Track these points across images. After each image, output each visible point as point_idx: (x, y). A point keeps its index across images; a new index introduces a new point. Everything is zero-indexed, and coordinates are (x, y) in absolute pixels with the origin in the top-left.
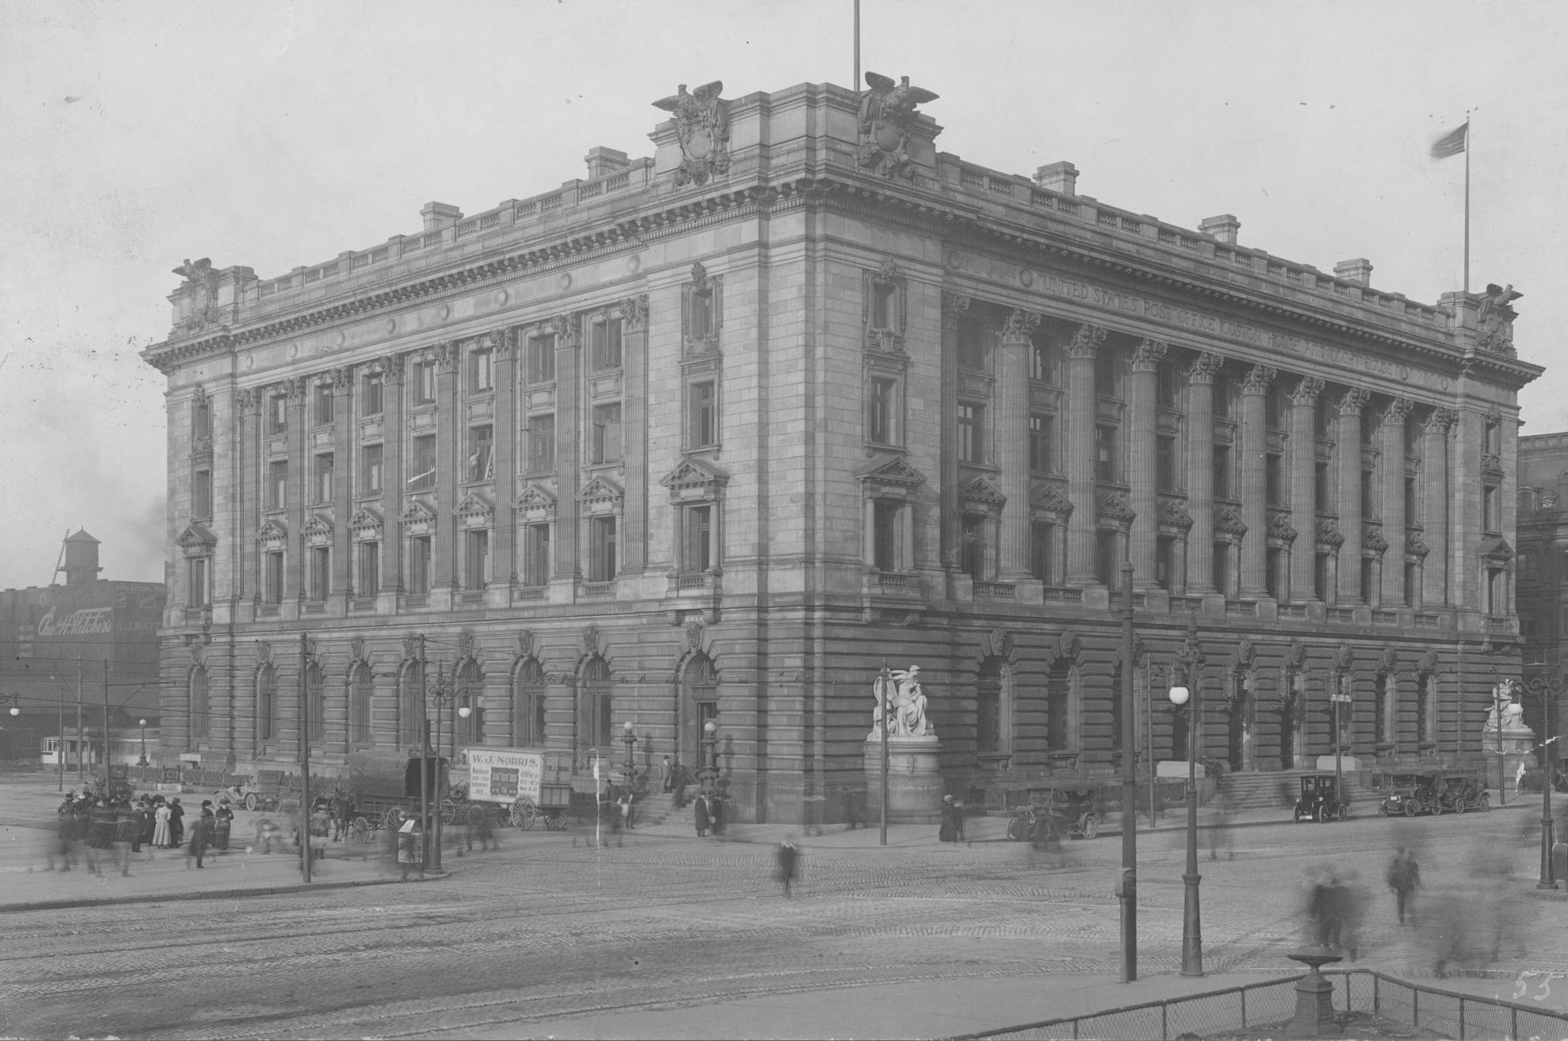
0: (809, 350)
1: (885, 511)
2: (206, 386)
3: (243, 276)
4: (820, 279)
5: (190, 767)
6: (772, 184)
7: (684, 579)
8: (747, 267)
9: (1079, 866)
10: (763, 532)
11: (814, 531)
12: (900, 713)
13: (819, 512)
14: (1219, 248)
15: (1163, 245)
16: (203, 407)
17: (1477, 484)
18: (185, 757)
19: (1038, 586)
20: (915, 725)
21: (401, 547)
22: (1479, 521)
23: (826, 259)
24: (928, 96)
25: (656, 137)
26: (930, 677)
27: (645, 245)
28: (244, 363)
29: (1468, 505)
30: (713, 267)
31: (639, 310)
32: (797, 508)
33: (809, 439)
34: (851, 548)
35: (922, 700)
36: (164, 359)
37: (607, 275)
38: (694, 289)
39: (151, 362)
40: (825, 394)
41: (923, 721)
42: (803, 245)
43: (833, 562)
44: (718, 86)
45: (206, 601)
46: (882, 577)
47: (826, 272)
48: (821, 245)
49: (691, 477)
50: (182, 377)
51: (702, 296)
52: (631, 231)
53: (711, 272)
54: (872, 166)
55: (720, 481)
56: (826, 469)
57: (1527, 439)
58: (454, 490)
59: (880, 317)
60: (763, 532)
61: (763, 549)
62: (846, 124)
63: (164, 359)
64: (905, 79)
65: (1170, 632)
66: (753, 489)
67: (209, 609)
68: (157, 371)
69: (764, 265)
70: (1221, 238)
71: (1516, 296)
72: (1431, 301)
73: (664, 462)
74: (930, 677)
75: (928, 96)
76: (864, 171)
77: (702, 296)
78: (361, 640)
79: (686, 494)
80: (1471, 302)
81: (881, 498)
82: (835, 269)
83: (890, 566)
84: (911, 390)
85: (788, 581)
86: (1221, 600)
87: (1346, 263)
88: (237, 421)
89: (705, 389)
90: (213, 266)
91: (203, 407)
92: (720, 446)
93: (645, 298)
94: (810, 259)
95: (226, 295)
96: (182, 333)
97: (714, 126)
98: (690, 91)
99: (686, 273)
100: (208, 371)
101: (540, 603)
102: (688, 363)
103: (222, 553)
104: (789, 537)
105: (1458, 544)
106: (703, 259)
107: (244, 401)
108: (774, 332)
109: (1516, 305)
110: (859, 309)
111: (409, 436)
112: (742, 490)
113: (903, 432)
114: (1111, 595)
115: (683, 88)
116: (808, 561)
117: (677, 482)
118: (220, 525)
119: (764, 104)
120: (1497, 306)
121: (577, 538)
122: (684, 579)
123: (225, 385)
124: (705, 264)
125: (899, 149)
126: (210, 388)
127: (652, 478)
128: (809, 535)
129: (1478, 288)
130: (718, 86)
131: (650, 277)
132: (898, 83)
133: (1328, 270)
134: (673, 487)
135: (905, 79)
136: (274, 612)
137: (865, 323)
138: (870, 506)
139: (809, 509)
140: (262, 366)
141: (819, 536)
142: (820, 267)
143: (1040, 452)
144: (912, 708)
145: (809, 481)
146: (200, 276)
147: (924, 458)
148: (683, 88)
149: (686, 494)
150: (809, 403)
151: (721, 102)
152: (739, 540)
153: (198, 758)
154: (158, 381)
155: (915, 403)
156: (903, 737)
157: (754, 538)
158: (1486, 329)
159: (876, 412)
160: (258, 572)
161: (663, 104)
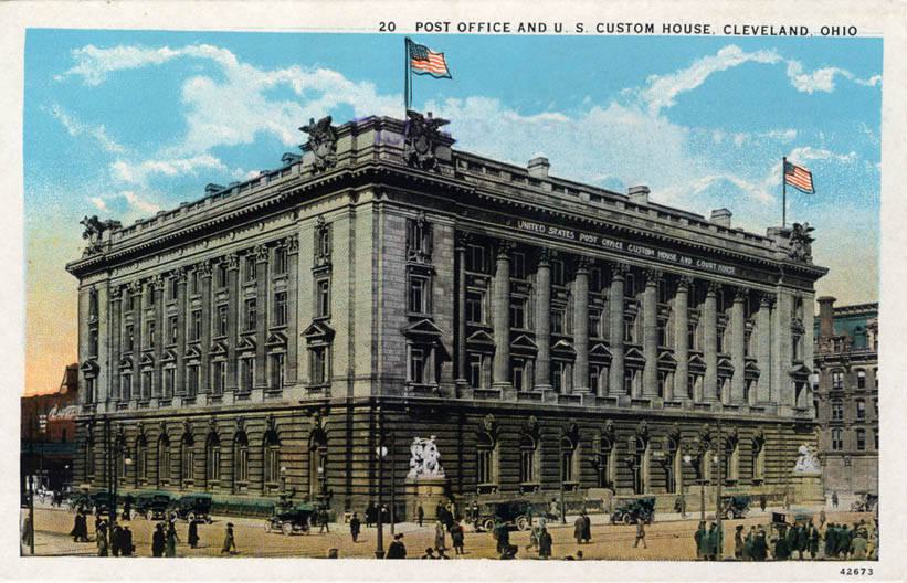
0: (375, 263)
4: (381, 222)
5: (83, 492)
7: (313, 389)
8: (343, 217)
10: (351, 362)
11: (377, 361)
12: (425, 463)
13: (380, 351)
15: (593, 203)
16: (94, 296)
17: (789, 333)
18: (83, 486)
20: (433, 468)
21: (185, 371)
22: (790, 355)
23: (384, 212)
25: (307, 148)
29: (784, 346)
31: (295, 243)
32: (368, 350)
33: (375, 311)
34: (399, 371)
35: (437, 454)
36: (80, 272)
37: (278, 226)
40: (383, 286)
41: (437, 467)
42: (371, 205)
43: (388, 379)
45: (94, 401)
47: (384, 220)
50: (85, 282)
51: (324, 231)
52: (291, 202)
54: (415, 172)
56: (383, 327)
57: (837, 310)
58: (209, 340)
59: (321, 246)
60: (351, 362)
61: (351, 373)
62: (397, 139)
63: (80, 272)
66: (346, 339)
69: (353, 216)
70: (721, 222)
71: (811, 229)
72: (762, 232)
73: (305, 323)
77: (324, 231)
78: (272, 417)
80: (785, 234)
82: (390, 217)
84: (435, 284)
85: (362, 391)
86: (628, 399)
88: (110, 304)
91: (94, 296)
94: (375, 212)
96: (86, 256)
98: (316, 122)
101: (248, 401)
102: (318, 271)
103: (103, 372)
104: (364, 368)
105: (778, 367)
108: (358, 253)
109: (812, 235)
110: (404, 239)
111: (189, 311)
112: (341, 339)
113: (430, 308)
114: (560, 397)
115: (312, 121)
116: (373, 378)
118: (101, 362)
119: (354, 129)
120: (801, 236)
121: (265, 366)
122: (313, 389)
123: (104, 284)
126: (98, 286)
127: (300, 332)
128: (374, 365)
129: (789, 227)
132: (426, 116)
133: (708, 218)
135: (430, 114)
136: (125, 407)
137: (407, 248)
139: (374, 349)
140: (127, 275)
142: (381, 217)
143: (515, 318)
145: (374, 335)
146: (94, 226)
147: (443, 325)
148: (312, 121)
150: (374, 290)
152: (340, 369)
153: (88, 486)
154: (74, 281)
155: (438, 291)
156: (429, 475)
157: (346, 366)
158: (794, 248)
159: (414, 298)
160: (119, 386)
161: (304, 129)
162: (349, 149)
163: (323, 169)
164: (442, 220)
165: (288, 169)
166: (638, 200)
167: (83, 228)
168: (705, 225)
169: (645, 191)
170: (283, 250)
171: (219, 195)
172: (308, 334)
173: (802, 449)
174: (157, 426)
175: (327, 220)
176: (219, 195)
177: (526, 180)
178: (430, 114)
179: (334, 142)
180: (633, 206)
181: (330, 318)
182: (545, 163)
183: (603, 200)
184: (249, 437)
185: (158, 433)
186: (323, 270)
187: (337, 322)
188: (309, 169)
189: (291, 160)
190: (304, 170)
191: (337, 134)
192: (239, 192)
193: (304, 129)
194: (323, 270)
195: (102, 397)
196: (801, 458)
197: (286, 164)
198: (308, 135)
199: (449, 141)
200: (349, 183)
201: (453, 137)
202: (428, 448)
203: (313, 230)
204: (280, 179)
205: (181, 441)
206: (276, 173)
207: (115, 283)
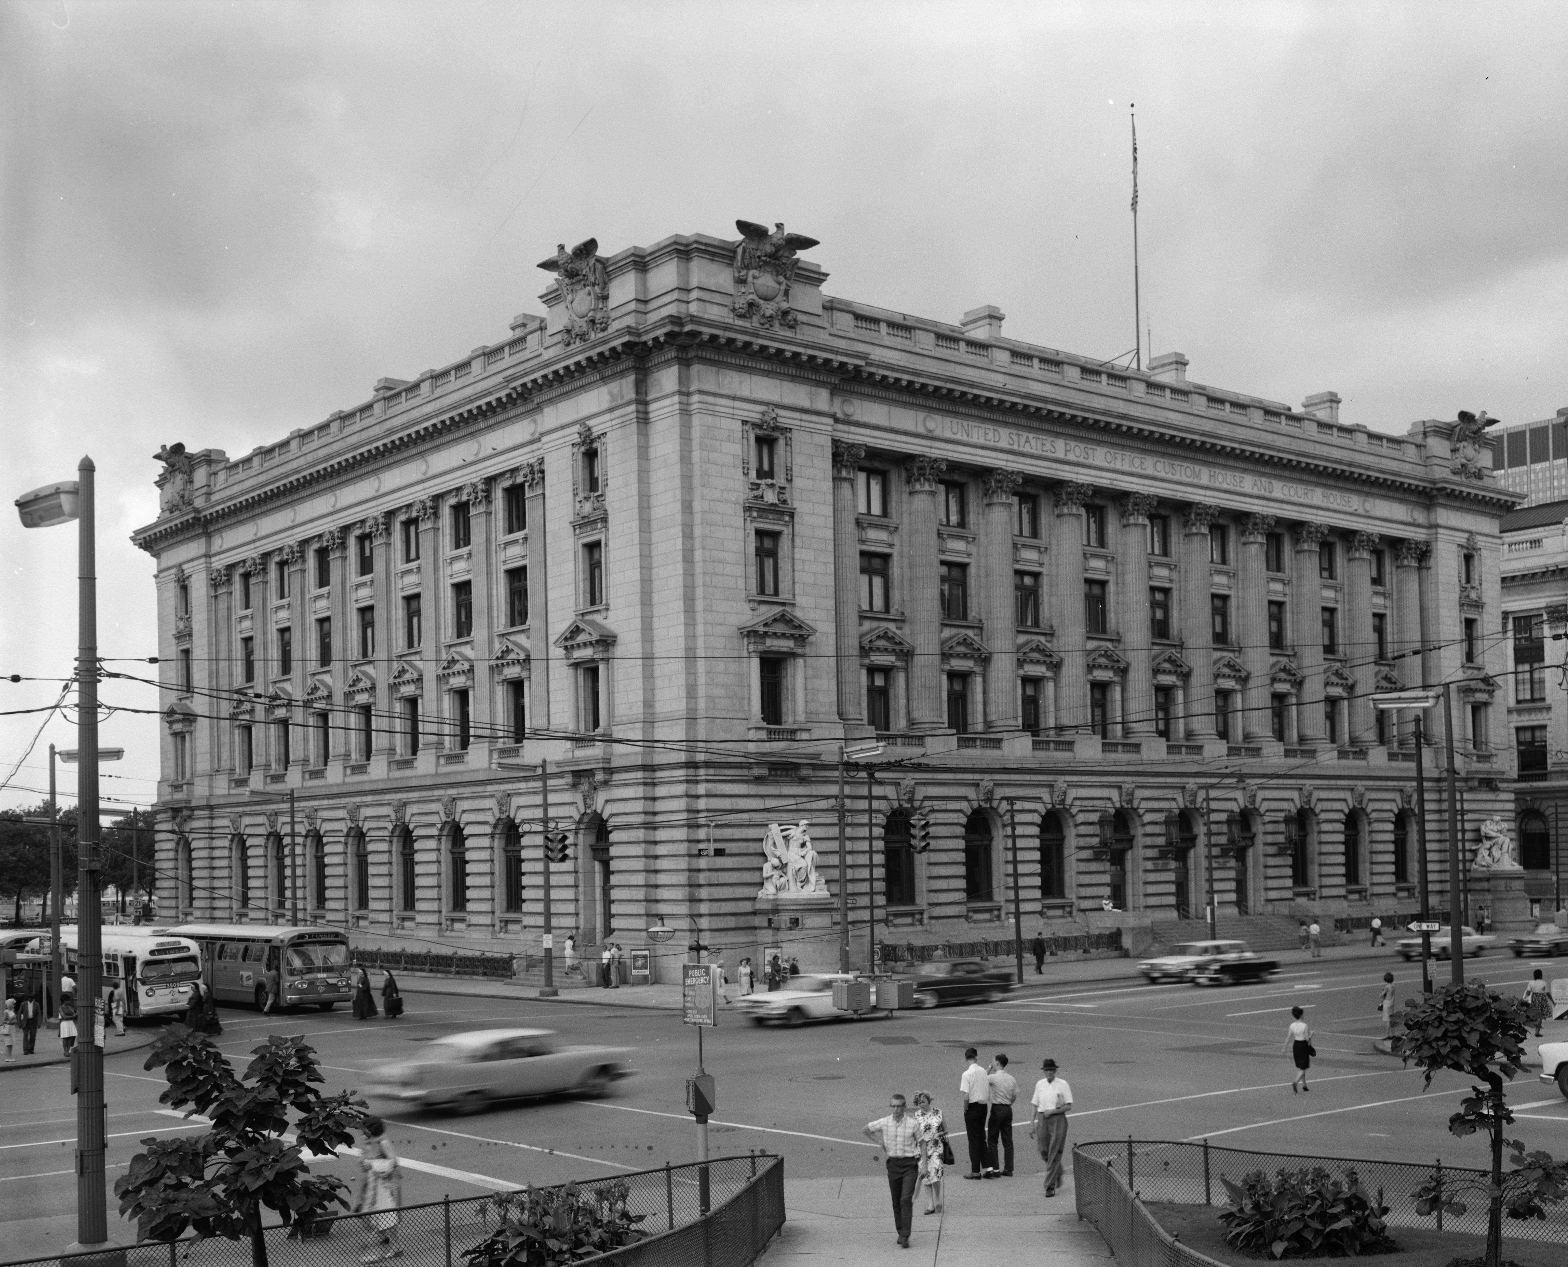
1: (773, 668)
2: (185, 567)
3: (209, 458)
6: (644, 338)
9: (1264, 982)
12: (790, 870)
14: (1323, 426)
19: (1279, 748)
20: (806, 881)
24: (808, 243)
25: (551, 298)
26: (819, 832)
27: (539, 408)
28: (218, 543)
30: (597, 426)
31: (537, 473)
35: (810, 852)
37: (502, 446)
38: (583, 449)
39: (141, 546)
44: (590, 246)
46: (770, 732)
48: (695, 398)
49: (582, 638)
52: (523, 398)
53: (596, 431)
54: (737, 318)
55: (607, 642)
62: (721, 277)
64: (1484, 413)
65: (1390, 783)
67: (190, 784)
68: (147, 554)
70: (1322, 414)
74: (819, 832)
75: (808, 243)
76: (739, 322)
79: (578, 654)
81: (765, 652)
83: (778, 721)
87: (840, 301)
89: (593, 547)
90: (187, 450)
92: (607, 605)
93: (541, 461)
95: (200, 476)
97: (594, 285)
98: (569, 250)
99: (573, 434)
100: (188, 552)
106: (590, 417)
107: (219, 581)
115: (561, 247)
117: (568, 644)
119: (640, 262)
124: (590, 423)
125: (779, 298)
127: (552, 639)
128: (691, 692)
130: (590, 246)
131: (545, 439)
132: (772, 230)
133: (1297, 410)
134: (566, 648)
135: (779, 226)
138: (755, 663)
140: (239, 542)
141: (701, 691)
144: (802, 863)
148: (561, 247)
149: (578, 654)
151: (599, 260)
154: (147, 562)
162: (632, 296)
163: (583, 337)
164: (1155, 756)
165: (522, 340)
166: (1166, 377)
167: (159, 467)
168: (1297, 419)
169: (1181, 363)
170: (517, 496)
171: (399, 394)
172: (566, 639)
173: (1488, 828)
174: (341, 813)
175: (596, 431)
176: (399, 394)
177: (962, 345)
178: (779, 226)
179: (605, 285)
180: (1161, 387)
181: (607, 609)
182: (995, 317)
183: (1184, 750)
184: (466, 832)
185: (343, 826)
186: (592, 522)
187: (621, 616)
188: (558, 338)
189: (525, 329)
190: (548, 341)
191: (608, 270)
192: (434, 388)
193: (548, 265)
194: (592, 522)
195: (203, 765)
196: (1488, 844)
197: (519, 333)
198: (554, 275)
199: (816, 277)
200: (636, 357)
201: (823, 270)
202: (794, 845)
203: (568, 450)
204: (508, 360)
205: (492, 836)
206: (500, 349)
207: (219, 563)
